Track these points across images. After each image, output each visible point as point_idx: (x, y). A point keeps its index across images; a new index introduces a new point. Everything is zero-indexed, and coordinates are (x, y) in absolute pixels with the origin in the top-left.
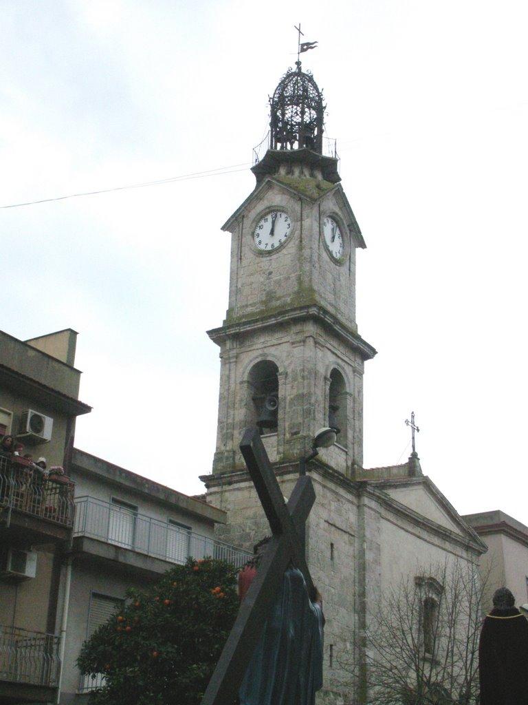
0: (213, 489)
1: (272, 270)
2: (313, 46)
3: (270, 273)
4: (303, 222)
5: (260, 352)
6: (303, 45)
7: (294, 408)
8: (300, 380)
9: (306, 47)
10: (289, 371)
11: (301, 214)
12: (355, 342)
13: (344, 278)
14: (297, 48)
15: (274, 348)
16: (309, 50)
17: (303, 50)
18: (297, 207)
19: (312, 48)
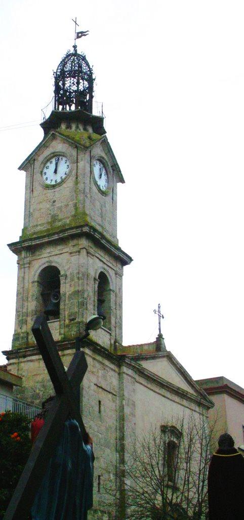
1: (55, 199)
2: (86, 34)
3: (54, 202)
6: (78, 33)
8: (76, 280)
9: (80, 35)
10: (68, 273)
14: (74, 36)
17: (78, 37)
19: (85, 35)
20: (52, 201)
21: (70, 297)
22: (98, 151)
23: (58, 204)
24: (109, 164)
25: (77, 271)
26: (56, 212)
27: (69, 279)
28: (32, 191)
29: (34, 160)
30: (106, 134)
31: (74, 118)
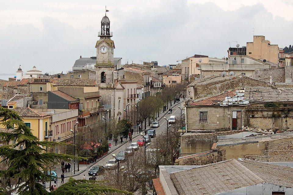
23: (104, 58)
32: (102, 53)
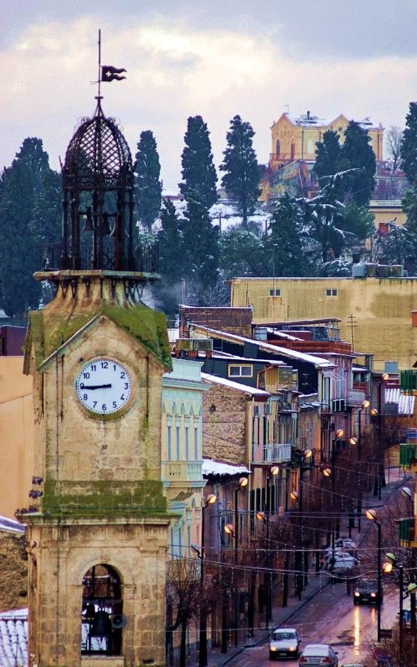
0: (215, 492)
1: (107, 444)
2: (120, 75)
3: (105, 447)
4: (149, 389)
5: (98, 552)
6: (105, 69)
7: (146, 631)
8: (153, 598)
9: (110, 74)
10: (139, 583)
11: (147, 377)
12: (300, 348)
13: (130, 561)
14: (96, 74)
15: (116, 551)
16: (114, 81)
17: (105, 79)
18: (142, 365)
19: (119, 79)
20: (100, 445)
21: (143, 623)
22: (65, 290)
23: (111, 454)
24: (150, 326)
25: (155, 584)
26: (107, 467)
27: (139, 594)
28: (62, 416)
29: (63, 357)
30: (183, 169)
31: (192, 407)
32: (93, 416)
